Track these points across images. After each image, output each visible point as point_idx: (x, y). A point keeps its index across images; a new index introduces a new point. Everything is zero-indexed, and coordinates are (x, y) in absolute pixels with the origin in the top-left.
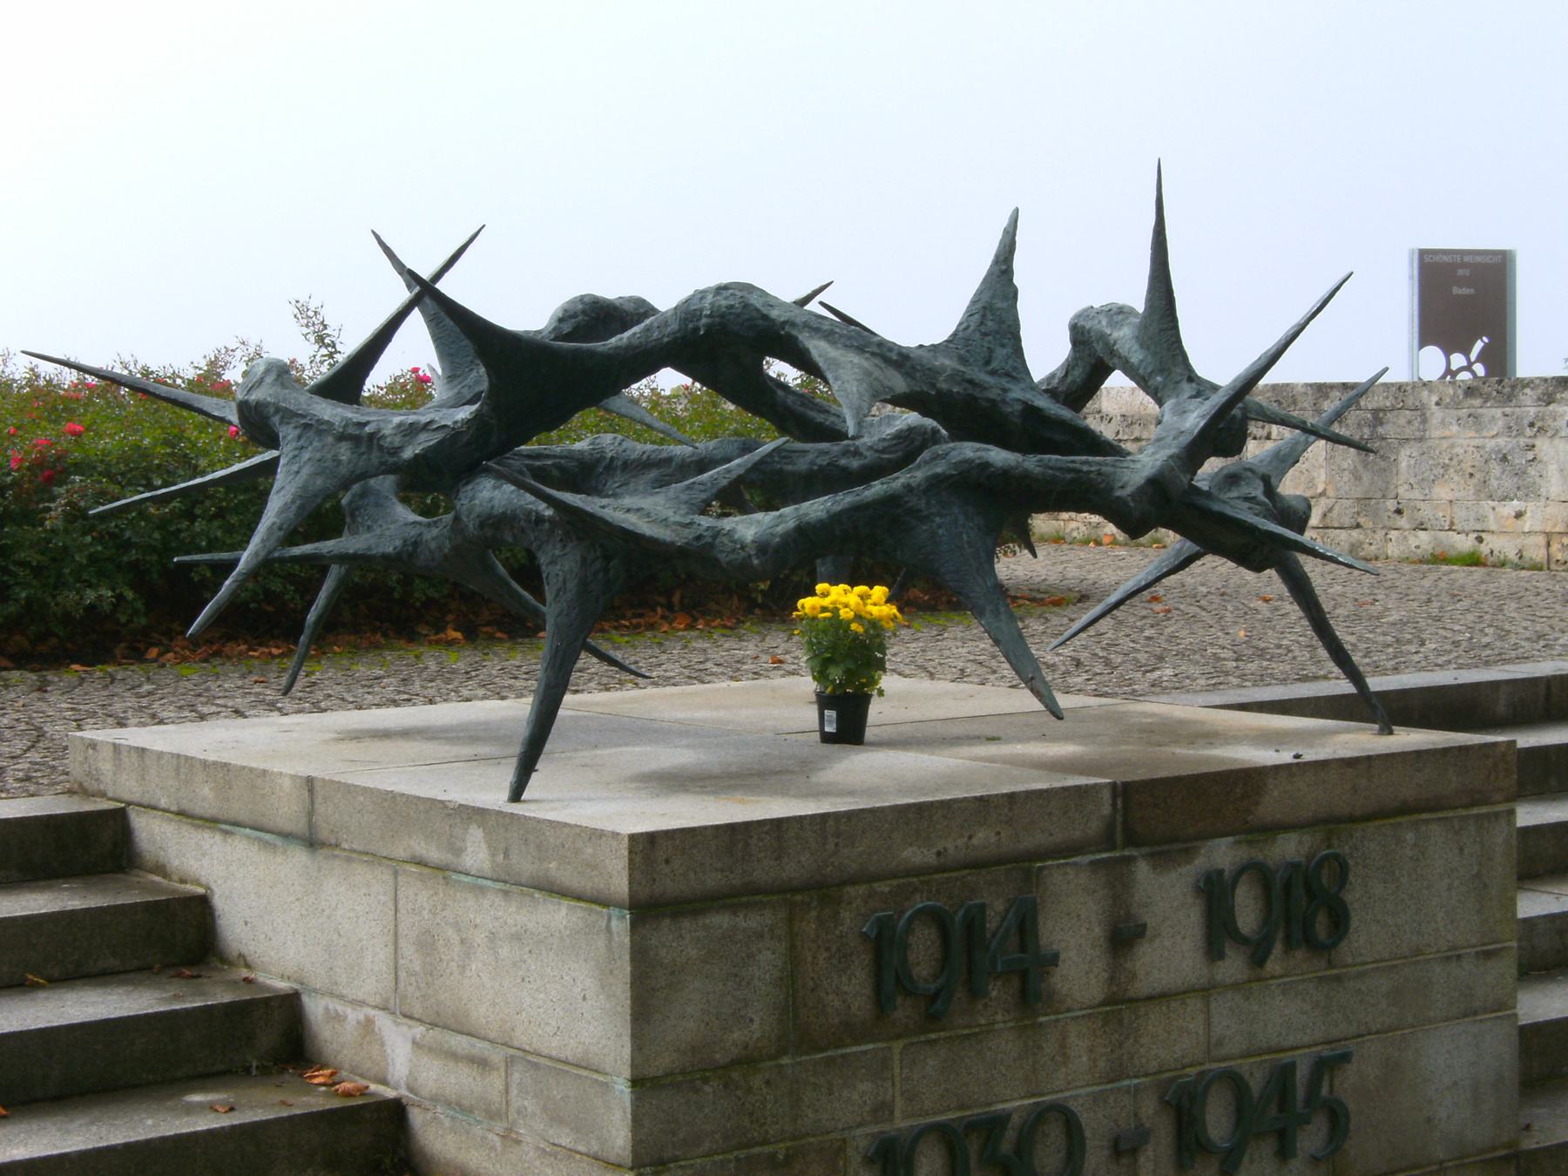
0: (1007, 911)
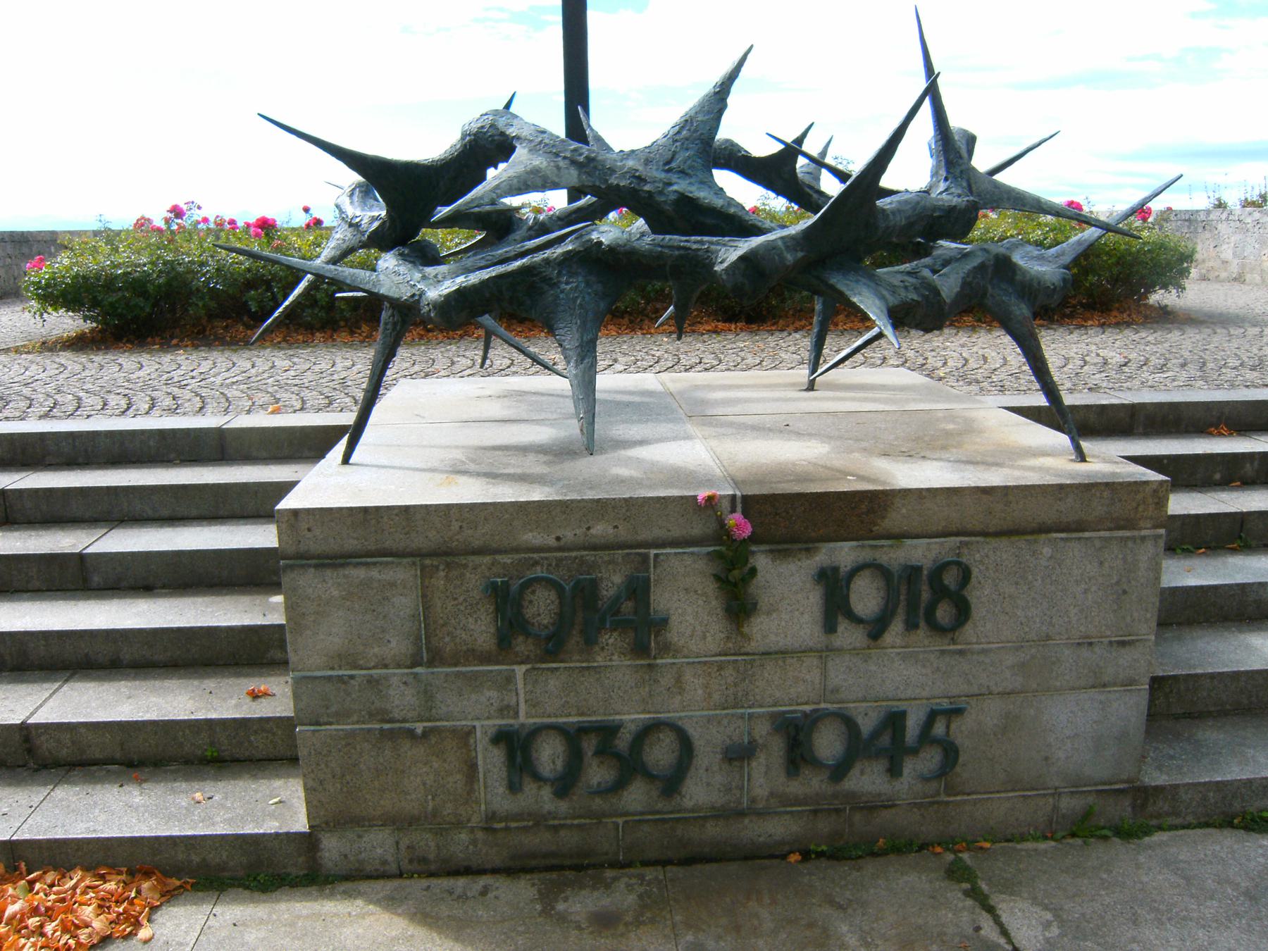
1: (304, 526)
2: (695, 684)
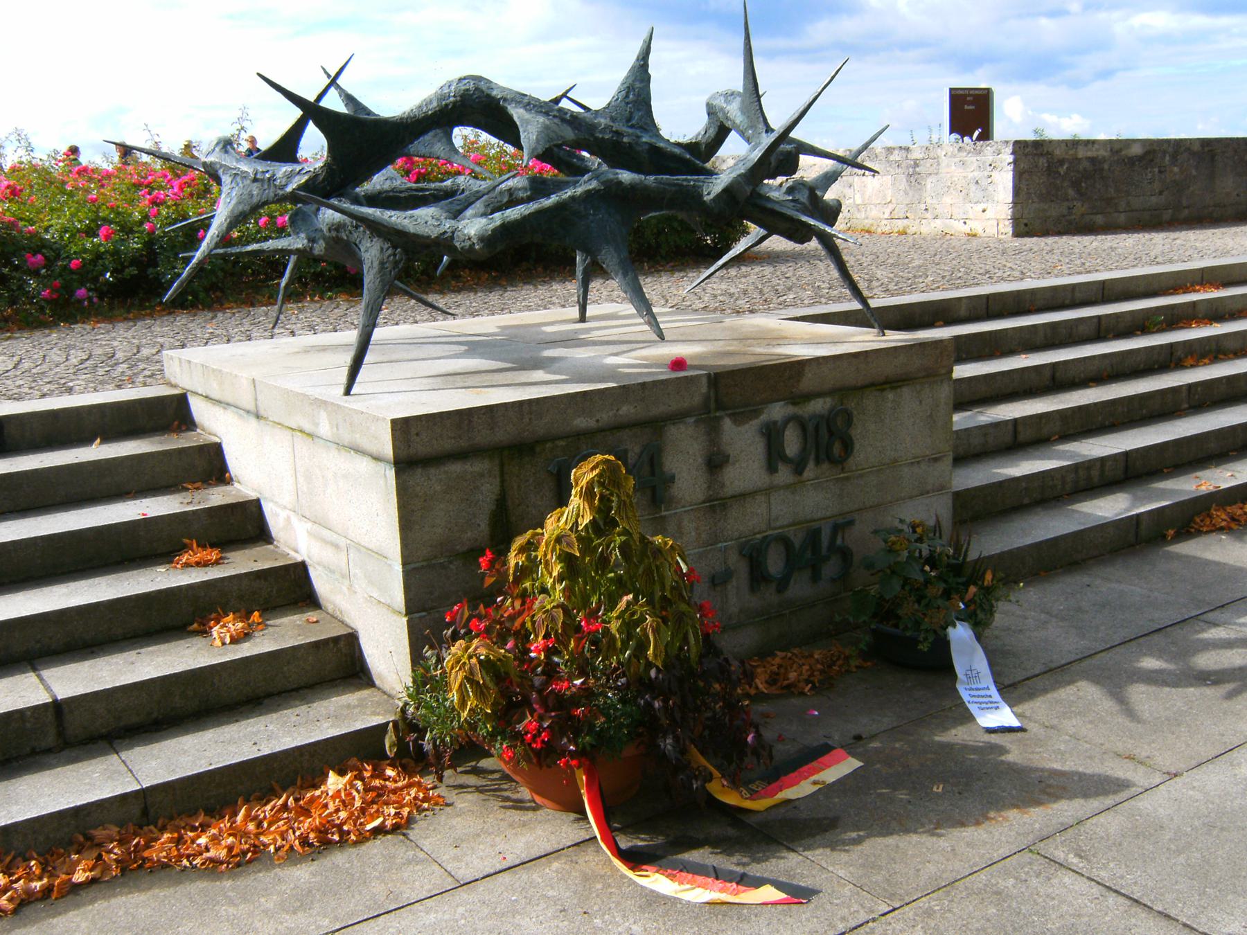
0: (642, 452)
1: (413, 431)
2: (689, 526)
